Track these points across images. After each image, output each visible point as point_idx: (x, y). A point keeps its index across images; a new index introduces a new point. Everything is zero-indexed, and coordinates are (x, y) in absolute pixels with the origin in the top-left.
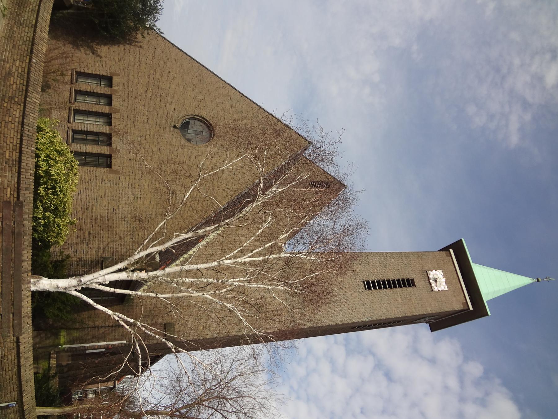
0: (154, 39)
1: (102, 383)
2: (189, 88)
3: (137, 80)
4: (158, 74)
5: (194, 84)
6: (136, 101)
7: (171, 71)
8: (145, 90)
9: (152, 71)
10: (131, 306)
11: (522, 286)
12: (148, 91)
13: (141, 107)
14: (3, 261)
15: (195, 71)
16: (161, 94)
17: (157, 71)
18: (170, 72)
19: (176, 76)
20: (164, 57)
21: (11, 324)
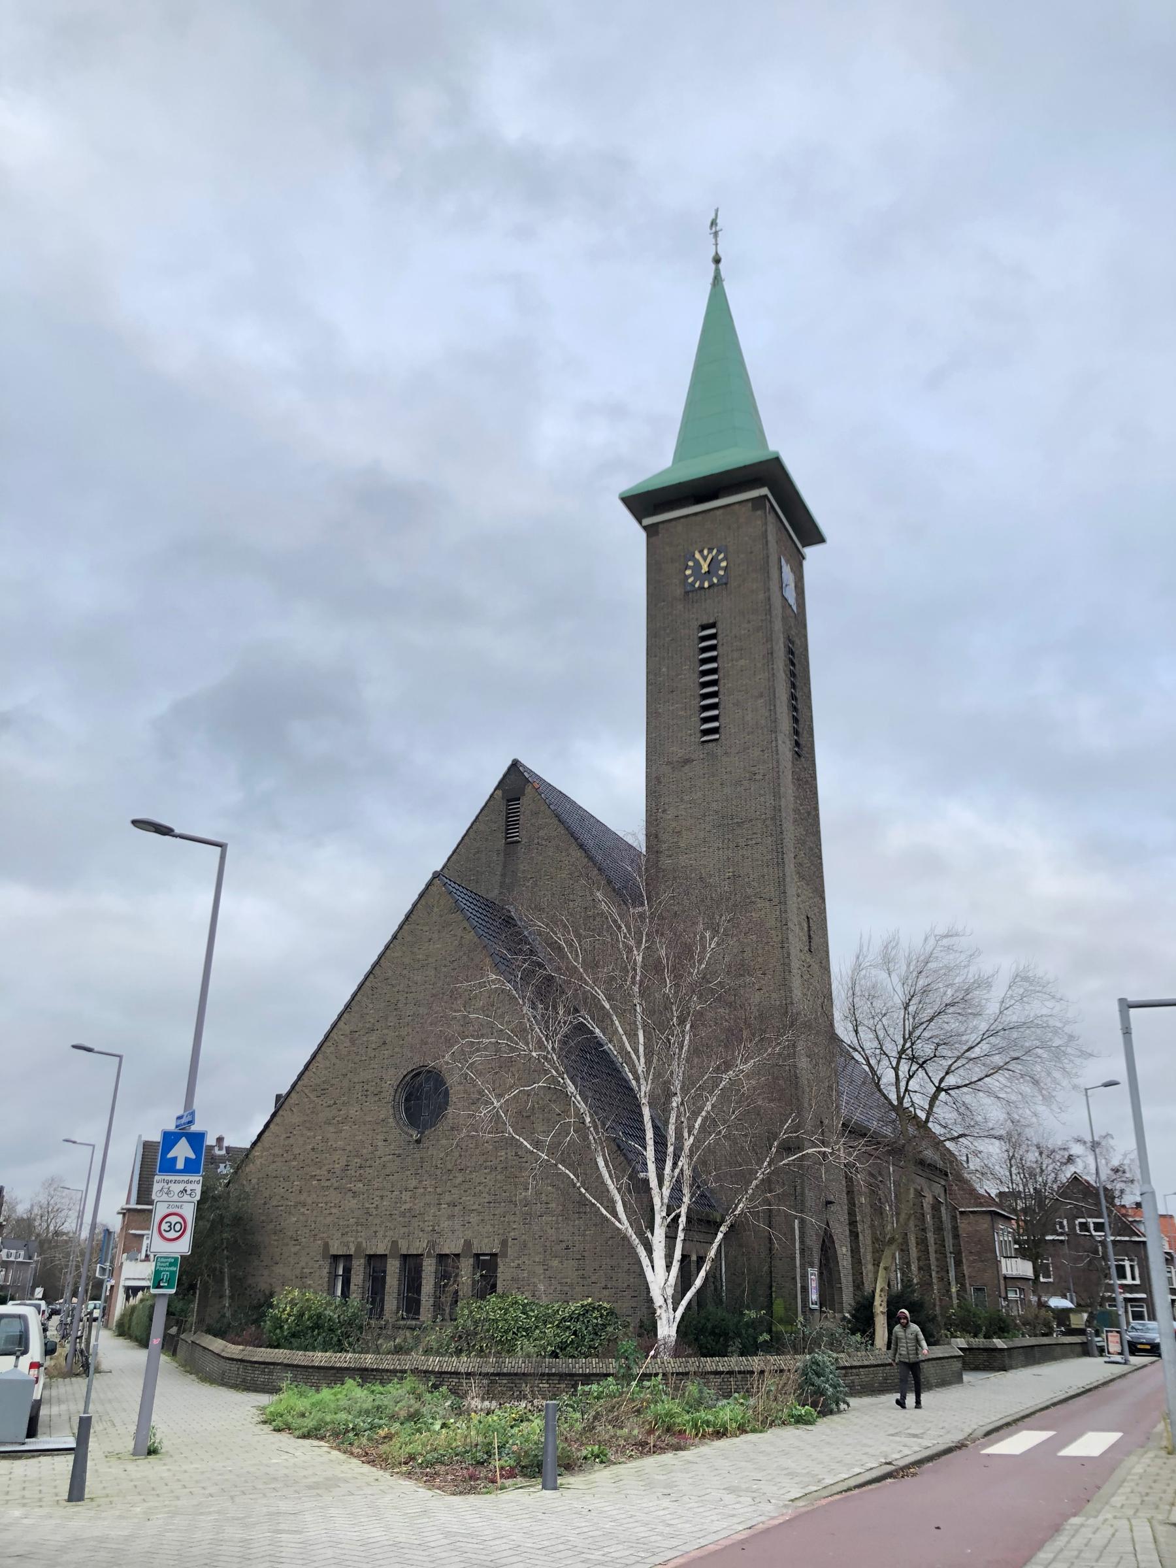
3: (334, 1211)
4: (318, 1172)
5: (332, 1102)
13: (385, 1203)
16: (358, 1165)
17: (314, 1173)
18: (313, 1149)
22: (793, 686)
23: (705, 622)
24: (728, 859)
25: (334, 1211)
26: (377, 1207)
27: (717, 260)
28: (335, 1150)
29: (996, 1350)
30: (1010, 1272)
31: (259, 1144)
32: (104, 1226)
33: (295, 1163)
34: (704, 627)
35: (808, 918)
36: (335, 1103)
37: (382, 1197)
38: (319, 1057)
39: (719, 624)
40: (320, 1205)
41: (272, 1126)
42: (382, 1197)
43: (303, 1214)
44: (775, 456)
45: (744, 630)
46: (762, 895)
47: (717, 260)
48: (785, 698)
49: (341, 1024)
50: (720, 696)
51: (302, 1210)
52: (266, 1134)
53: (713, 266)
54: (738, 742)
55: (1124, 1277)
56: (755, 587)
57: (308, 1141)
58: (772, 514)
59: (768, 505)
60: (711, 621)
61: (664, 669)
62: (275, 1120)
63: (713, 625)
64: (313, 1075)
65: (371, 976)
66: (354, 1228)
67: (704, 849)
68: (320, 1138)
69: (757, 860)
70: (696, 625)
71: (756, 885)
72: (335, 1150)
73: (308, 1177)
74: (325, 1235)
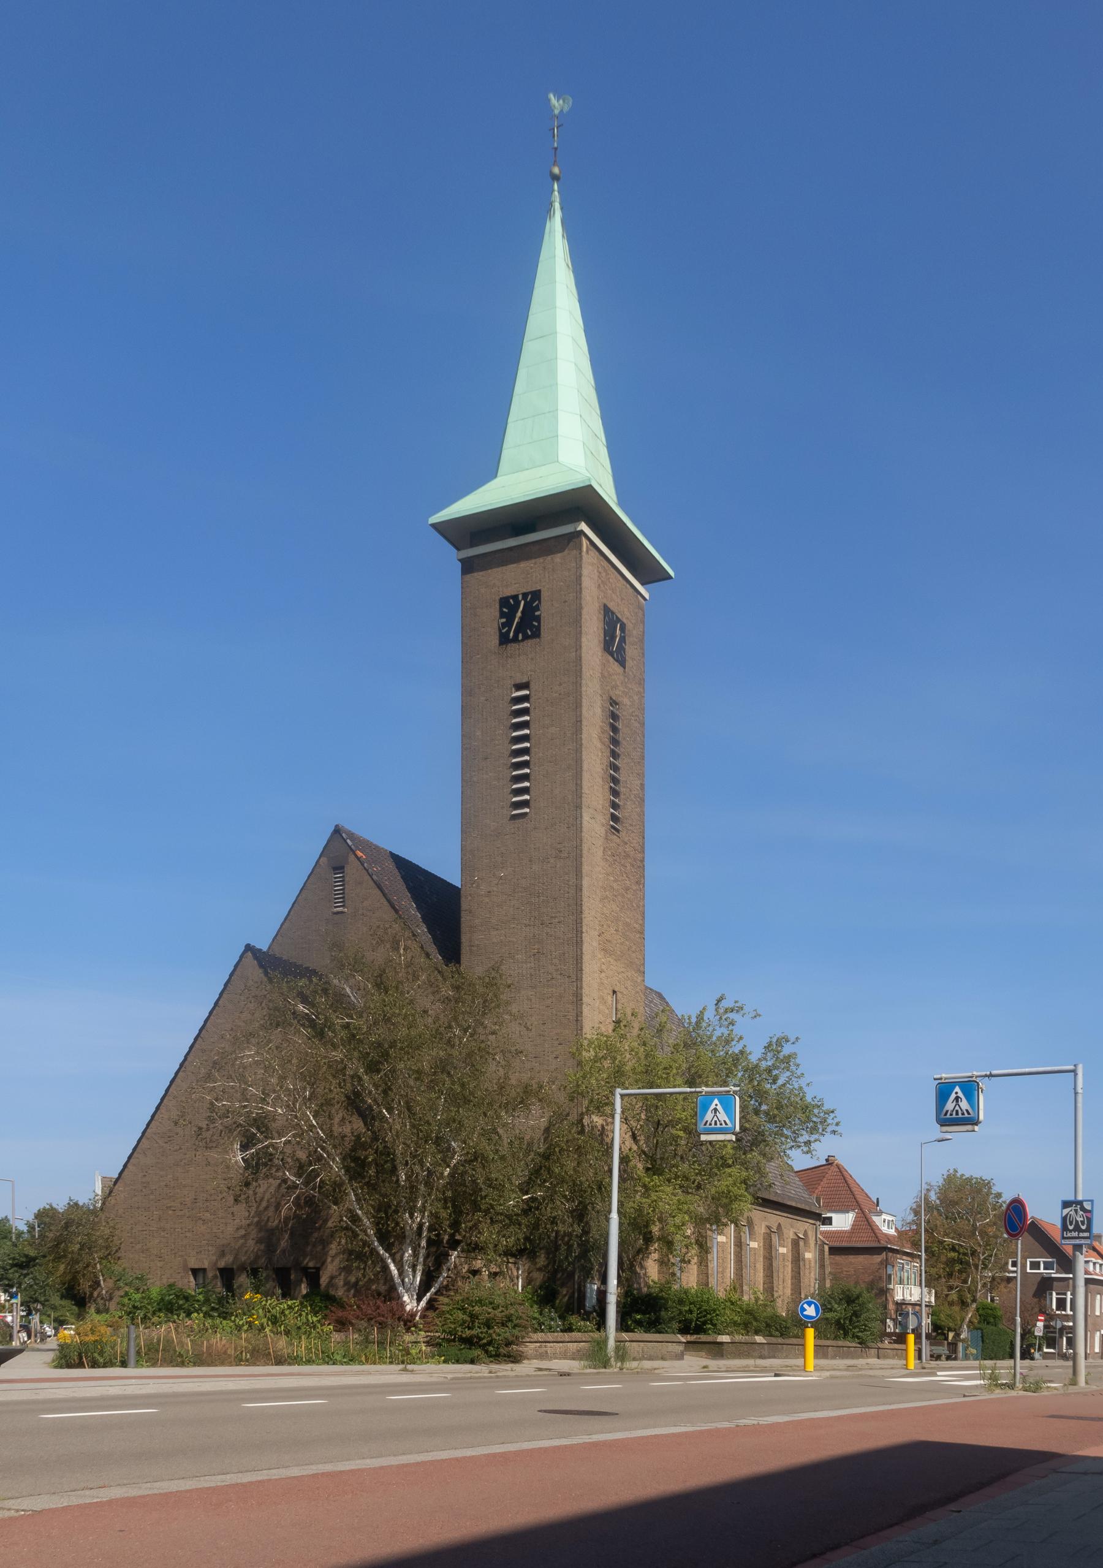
0: (116, 1209)
1: (201, 1269)
2: (187, 1156)
3: (188, 1234)
4: (172, 1204)
5: (178, 1147)
6: (221, 1237)
7: (164, 1183)
8: (202, 1222)
9: (170, 1212)
10: (686, 1293)
11: (582, 485)
12: (203, 1218)
13: (229, 1229)
14: (198, 1475)
15: (156, 1145)
16: (205, 1199)
17: (169, 1205)
18: (166, 1186)
19: (171, 1176)
20: (143, 1194)
21: (576, 1287)
22: (614, 755)
23: (518, 681)
24: (534, 936)
25: (188, 1234)
26: (222, 1232)
28: (185, 1186)
29: (721, 1343)
30: (909, 1298)
31: (120, 1181)
32: (843, 1292)
33: (152, 1197)
34: (519, 687)
35: (614, 992)
36: (180, 1149)
37: (226, 1224)
38: (163, 1109)
39: (532, 685)
40: (177, 1230)
41: (129, 1166)
42: (226, 1224)
43: (164, 1237)
44: (587, 483)
45: (556, 693)
46: (562, 972)
48: (600, 770)
49: (178, 1080)
50: (531, 767)
51: (163, 1234)
52: (125, 1173)
54: (546, 817)
55: (1065, 1310)
56: (567, 644)
57: (161, 1179)
58: (593, 552)
59: (585, 542)
60: (525, 680)
61: (479, 733)
62: (131, 1161)
63: (525, 686)
64: (159, 1124)
65: (199, 1039)
66: (206, 1248)
67: (513, 926)
68: (171, 1176)
69: (559, 938)
70: (509, 683)
71: (558, 962)
72: (185, 1186)
73: (164, 1208)
74: (183, 1253)
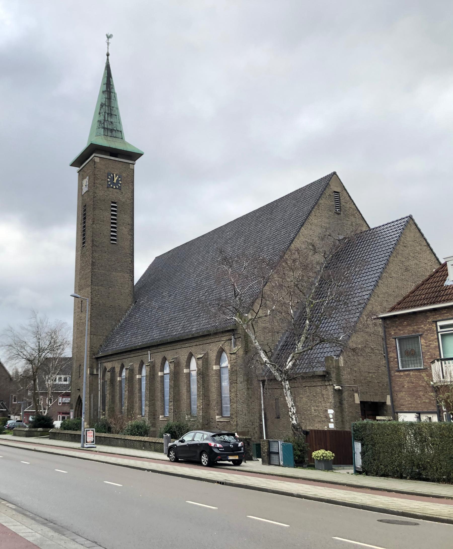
27: (108, 55)
47: (108, 55)
53: (106, 57)
